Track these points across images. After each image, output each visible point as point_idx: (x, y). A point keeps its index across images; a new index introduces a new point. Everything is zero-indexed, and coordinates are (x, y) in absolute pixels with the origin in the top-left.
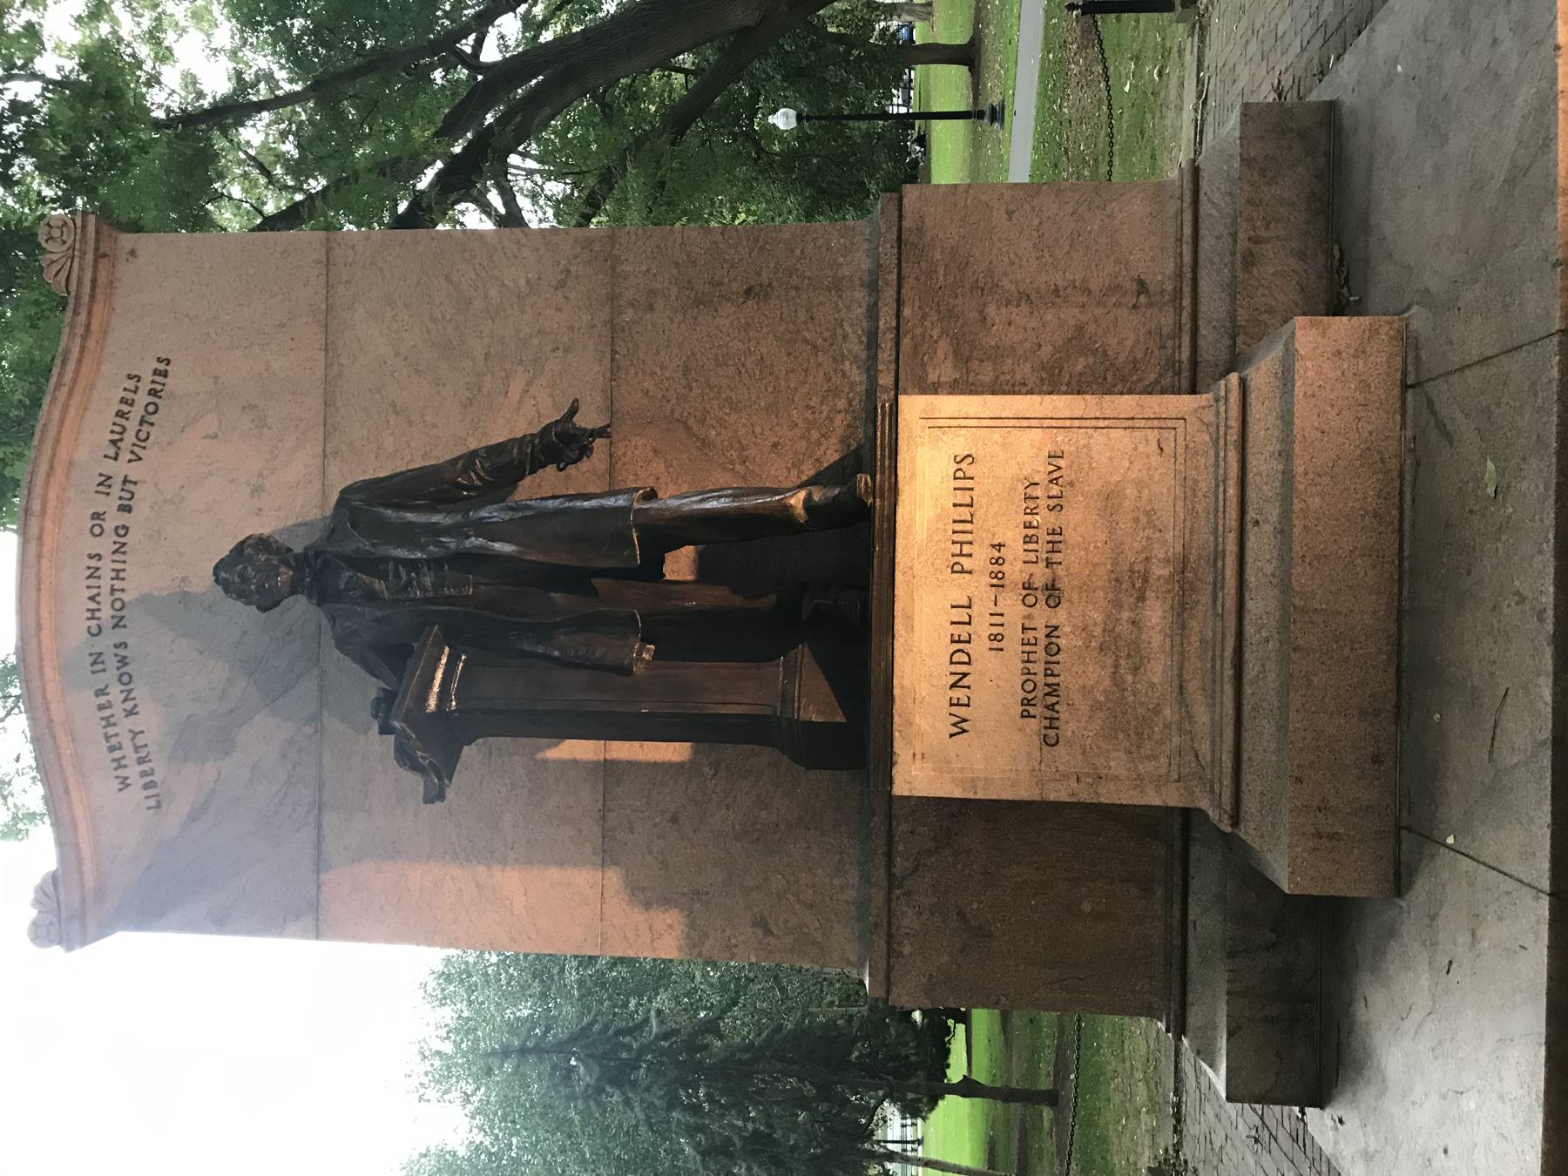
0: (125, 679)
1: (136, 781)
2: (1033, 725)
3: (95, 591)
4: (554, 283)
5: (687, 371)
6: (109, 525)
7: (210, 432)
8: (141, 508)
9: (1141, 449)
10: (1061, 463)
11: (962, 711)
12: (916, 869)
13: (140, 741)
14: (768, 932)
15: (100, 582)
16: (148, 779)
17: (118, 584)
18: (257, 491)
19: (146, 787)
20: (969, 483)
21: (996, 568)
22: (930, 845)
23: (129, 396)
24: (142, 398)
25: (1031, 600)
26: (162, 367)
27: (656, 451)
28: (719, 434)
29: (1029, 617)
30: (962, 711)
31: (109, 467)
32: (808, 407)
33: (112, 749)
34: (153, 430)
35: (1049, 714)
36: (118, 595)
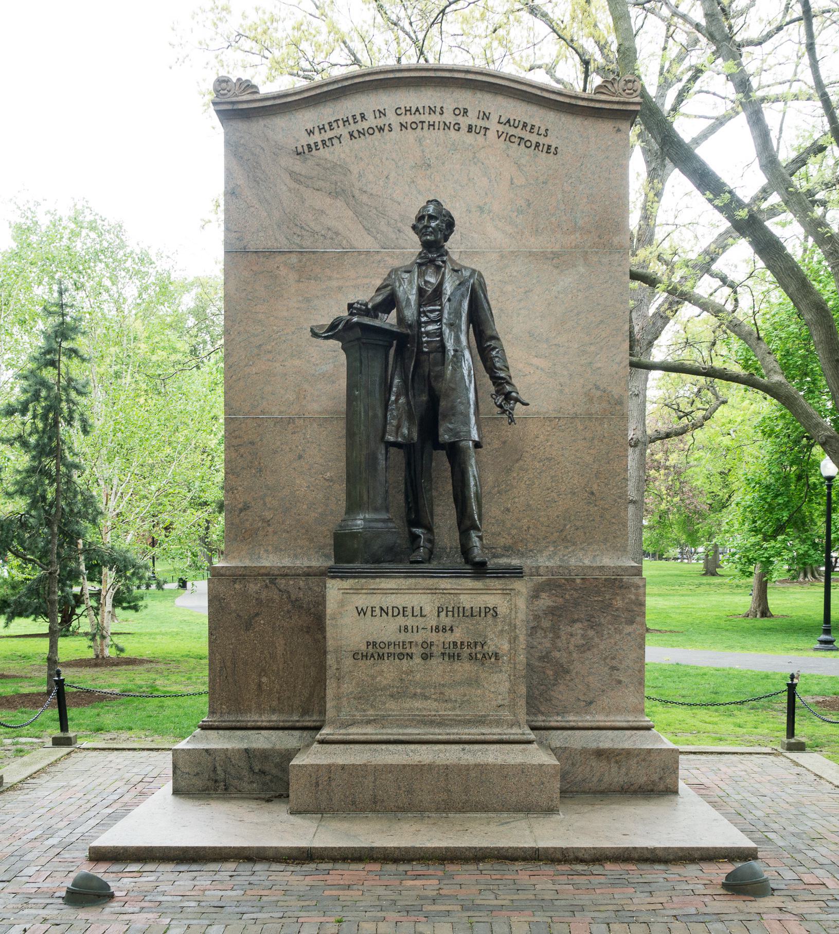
0: (371, 131)
1: (311, 140)
2: (363, 647)
3: (421, 111)
4: (598, 383)
5: (549, 459)
6: (460, 119)
7: (515, 181)
8: (470, 138)
9: (500, 697)
10: (493, 660)
11: (369, 612)
12: (280, 591)
13: (335, 141)
14: (241, 511)
15: (427, 114)
16: (313, 146)
17: (426, 125)
18: (481, 209)
19: (309, 146)
20: (483, 614)
21: (441, 628)
22: (293, 597)
23: (536, 130)
24: (534, 138)
25: (425, 646)
26: (553, 150)
27: (504, 442)
28: (514, 478)
29: (417, 644)
30: (369, 612)
31: (494, 118)
32: (529, 528)
33: (330, 124)
34: (515, 145)
35: (369, 655)
36: (420, 125)
